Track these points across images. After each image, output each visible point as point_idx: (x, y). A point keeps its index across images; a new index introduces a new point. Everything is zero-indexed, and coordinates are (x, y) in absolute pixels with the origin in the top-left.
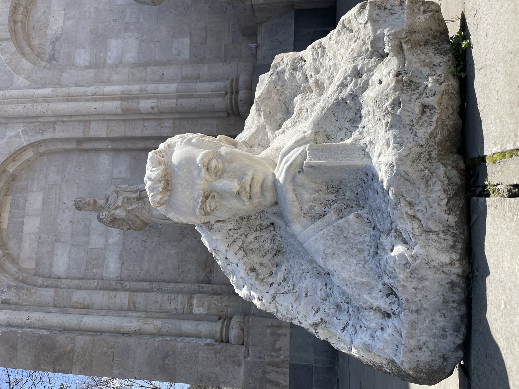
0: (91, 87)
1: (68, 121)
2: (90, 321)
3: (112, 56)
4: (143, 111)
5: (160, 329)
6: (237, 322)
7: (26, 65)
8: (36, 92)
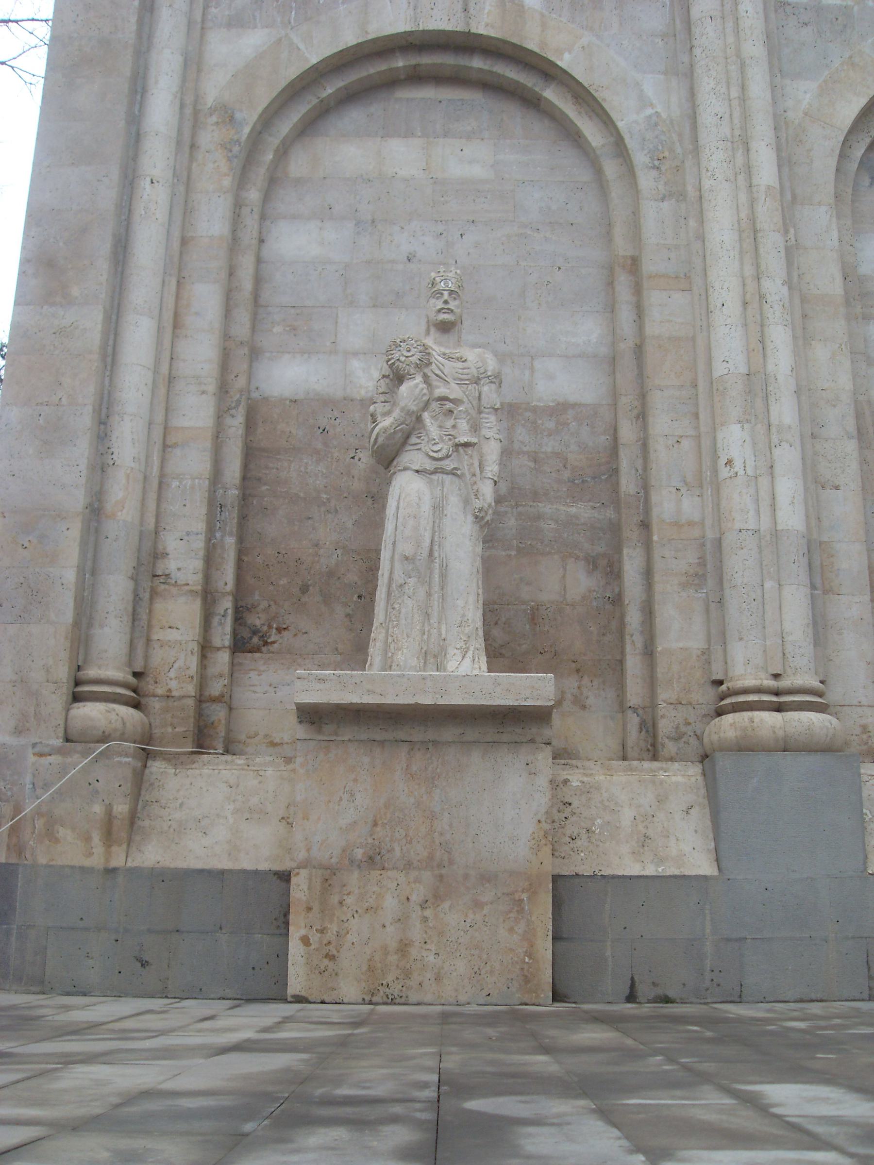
4: (720, 436)
6: (124, 724)
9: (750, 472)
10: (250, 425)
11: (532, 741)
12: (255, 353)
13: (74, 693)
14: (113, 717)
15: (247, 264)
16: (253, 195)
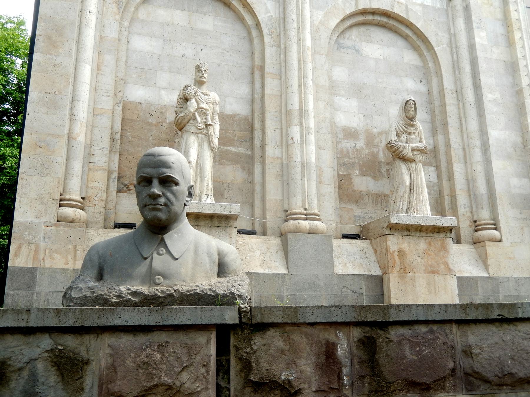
0: (311, 82)
1: (280, 59)
2: (86, 72)
3: (340, 101)
4: (289, 129)
5: (75, 139)
7: (334, 22)
8: (307, 32)
9: (299, 142)
10: (124, 110)
11: (231, 227)
12: (125, 83)
13: (60, 204)
14: (76, 213)
15: (450, 15)
16: (126, 23)
